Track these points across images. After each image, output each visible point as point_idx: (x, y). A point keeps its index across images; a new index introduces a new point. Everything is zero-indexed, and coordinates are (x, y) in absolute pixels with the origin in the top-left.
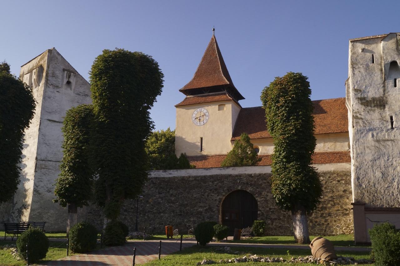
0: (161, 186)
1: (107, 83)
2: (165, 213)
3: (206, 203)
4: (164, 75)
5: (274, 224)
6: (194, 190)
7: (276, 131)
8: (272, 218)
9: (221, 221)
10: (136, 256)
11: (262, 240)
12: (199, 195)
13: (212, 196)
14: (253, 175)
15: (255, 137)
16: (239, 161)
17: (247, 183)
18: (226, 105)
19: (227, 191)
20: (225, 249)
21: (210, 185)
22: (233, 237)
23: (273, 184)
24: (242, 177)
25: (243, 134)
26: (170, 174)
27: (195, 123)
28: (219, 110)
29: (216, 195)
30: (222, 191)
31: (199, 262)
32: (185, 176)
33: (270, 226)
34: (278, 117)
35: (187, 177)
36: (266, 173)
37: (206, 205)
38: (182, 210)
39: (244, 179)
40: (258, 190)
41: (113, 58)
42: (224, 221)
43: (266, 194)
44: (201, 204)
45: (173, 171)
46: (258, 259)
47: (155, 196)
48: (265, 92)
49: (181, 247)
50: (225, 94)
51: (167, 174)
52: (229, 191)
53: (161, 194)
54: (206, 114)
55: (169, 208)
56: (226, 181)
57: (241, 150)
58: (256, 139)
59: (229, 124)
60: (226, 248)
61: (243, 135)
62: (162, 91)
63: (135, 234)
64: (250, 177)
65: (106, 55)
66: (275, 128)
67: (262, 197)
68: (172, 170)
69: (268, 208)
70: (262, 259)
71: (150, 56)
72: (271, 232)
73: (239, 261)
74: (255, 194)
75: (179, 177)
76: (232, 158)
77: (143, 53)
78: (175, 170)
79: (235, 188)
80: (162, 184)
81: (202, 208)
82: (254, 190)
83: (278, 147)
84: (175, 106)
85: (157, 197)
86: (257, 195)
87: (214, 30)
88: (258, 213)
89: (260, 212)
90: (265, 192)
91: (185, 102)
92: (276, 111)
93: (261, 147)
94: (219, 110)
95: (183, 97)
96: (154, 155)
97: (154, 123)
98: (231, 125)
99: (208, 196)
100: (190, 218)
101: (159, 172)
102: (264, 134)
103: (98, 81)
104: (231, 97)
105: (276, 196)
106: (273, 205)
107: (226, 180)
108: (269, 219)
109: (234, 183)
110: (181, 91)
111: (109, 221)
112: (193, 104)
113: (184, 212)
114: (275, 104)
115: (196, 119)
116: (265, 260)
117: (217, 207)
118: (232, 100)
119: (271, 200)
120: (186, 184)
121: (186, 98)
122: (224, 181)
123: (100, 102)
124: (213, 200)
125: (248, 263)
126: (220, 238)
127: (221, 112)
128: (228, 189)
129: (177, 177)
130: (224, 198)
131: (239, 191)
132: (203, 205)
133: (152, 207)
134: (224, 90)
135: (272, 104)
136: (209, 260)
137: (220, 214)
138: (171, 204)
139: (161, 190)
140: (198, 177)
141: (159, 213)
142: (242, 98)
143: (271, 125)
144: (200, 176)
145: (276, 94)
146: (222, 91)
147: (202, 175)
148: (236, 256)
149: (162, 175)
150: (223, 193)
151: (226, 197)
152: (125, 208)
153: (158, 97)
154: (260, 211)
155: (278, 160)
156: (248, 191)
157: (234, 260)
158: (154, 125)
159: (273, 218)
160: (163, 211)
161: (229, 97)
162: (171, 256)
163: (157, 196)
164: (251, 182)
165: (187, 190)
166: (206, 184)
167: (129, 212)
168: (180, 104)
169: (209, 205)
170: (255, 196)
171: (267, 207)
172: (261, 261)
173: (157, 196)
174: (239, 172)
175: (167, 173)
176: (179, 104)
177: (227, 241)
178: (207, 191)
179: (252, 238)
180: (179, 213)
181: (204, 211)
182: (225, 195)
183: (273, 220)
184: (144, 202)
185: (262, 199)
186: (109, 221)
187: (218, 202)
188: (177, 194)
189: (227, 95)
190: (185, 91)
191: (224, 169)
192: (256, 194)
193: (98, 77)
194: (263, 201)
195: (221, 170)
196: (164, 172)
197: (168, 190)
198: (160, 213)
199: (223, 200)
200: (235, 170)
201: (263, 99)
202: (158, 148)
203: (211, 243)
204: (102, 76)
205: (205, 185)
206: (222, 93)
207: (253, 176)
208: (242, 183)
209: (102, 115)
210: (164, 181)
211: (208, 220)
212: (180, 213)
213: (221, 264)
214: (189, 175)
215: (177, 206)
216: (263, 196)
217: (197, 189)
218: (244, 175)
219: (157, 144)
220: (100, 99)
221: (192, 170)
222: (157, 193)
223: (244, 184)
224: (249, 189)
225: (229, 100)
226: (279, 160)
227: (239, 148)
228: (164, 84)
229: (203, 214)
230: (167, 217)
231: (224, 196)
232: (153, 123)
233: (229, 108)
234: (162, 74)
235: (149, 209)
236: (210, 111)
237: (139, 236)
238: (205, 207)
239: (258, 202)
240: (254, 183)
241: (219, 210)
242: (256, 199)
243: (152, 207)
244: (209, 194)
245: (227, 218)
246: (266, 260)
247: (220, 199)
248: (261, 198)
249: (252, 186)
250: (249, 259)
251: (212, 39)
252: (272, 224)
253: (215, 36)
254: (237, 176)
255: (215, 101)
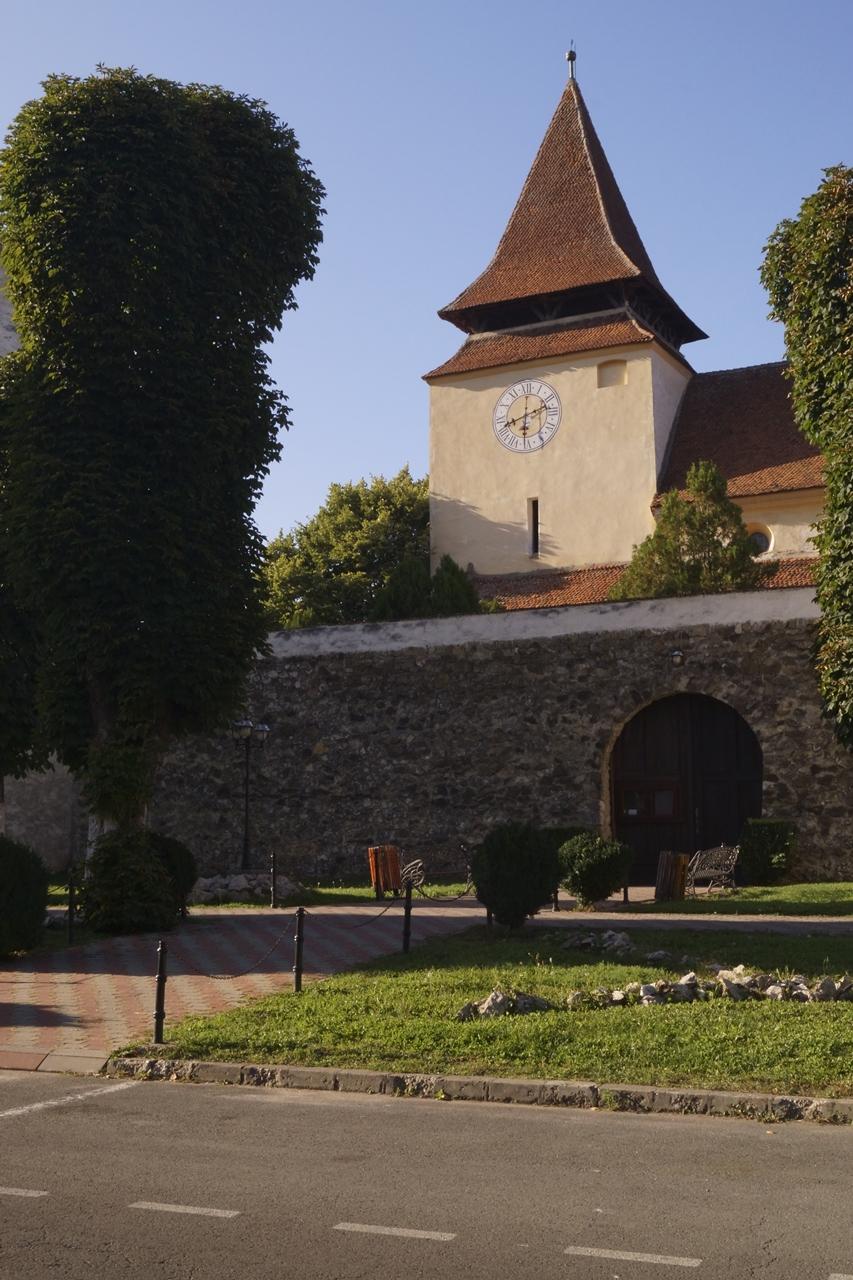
0: (360, 688)
1: (63, 221)
2: (376, 798)
3: (547, 754)
4: (324, 189)
5: (833, 831)
6: (494, 702)
7: (832, 417)
8: (822, 807)
9: (611, 825)
10: (169, 978)
11: (780, 898)
12: (515, 718)
13: (570, 723)
14: (738, 630)
15: (753, 489)
16: (681, 578)
17: (716, 666)
18: (629, 364)
19: (631, 700)
20: (605, 941)
21: (561, 679)
22: (654, 888)
23: (825, 650)
24: (692, 641)
25: (697, 466)
26: (394, 638)
27: (507, 442)
28: (599, 387)
29: (586, 719)
30: (610, 703)
31: (470, 1005)
32: (456, 643)
33: (816, 840)
34: (842, 351)
35: (462, 647)
36: (795, 620)
37: (543, 760)
38: (448, 782)
39: (701, 647)
40: (761, 690)
41: (85, 109)
42: (619, 821)
43: (796, 705)
44: (524, 759)
45: (405, 626)
46: (753, 984)
47: (336, 730)
48: (781, 245)
49: (407, 934)
50: (624, 318)
51: (381, 639)
52: (638, 701)
53: (362, 719)
54: (551, 403)
55: (395, 776)
56: (625, 661)
57: (688, 533)
58: (754, 495)
59: (643, 438)
60: (610, 937)
61: (697, 470)
62: (316, 260)
63: (240, 881)
64: (726, 639)
65: (56, 100)
66: (829, 402)
67: (778, 719)
68: (401, 623)
69: (804, 764)
70: (771, 987)
71: (256, 102)
72: (818, 868)
73: (660, 996)
74: (748, 707)
75: (431, 650)
76: (650, 567)
77: (226, 87)
78: (414, 622)
79: (666, 685)
80: (363, 679)
81: (526, 775)
82: (744, 694)
83: (845, 486)
84: (424, 378)
85: (345, 733)
86: (756, 713)
87: (572, 57)
88: (764, 788)
89: (772, 784)
90: (793, 700)
91: (463, 360)
92: (830, 324)
93: (777, 527)
94: (601, 384)
95: (453, 340)
96: (349, 577)
97: (286, 397)
98: (653, 443)
99: (551, 723)
100: (481, 813)
101: (348, 630)
102: (788, 474)
103: (26, 215)
104: (648, 330)
105: (837, 703)
106: (827, 753)
107: (627, 653)
108: (810, 810)
109: (658, 667)
110: (445, 315)
111: (109, 826)
112: (490, 367)
113: (454, 791)
114: (827, 294)
115: (508, 425)
116: (784, 993)
117: (590, 769)
118: (654, 342)
119: (818, 732)
120: (461, 676)
121: (468, 345)
122: (616, 659)
123: (43, 311)
124: (571, 738)
125: (705, 1004)
126: (594, 889)
127: (609, 391)
128: (634, 693)
129: (421, 649)
130: (618, 729)
131: (679, 697)
132: (531, 761)
133: (327, 774)
134: (621, 304)
135: (814, 293)
136: (518, 994)
137: (604, 798)
138: (403, 762)
139: (361, 704)
140: (510, 645)
141: (352, 799)
142: (696, 334)
143: (809, 391)
144: (516, 643)
145: (832, 244)
146: (612, 307)
147: (525, 636)
148: (649, 971)
149: (363, 642)
150: (613, 707)
151: (626, 725)
152: (219, 781)
153: (301, 290)
154: (773, 778)
155: (844, 543)
156: (719, 697)
157: (637, 990)
158: (285, 410)
159: (829, 806)
160: (372, 790)
161: (640, 330)
162: (354, 980)
163: (346, 729)
164: (731, 661)
165: (465, 702)
166: (542, 674)
167: (237, 795)
168: (443, 367)
169: (556, 760)
170: (748, 719)
171: (803, 761)
172: (764, 997)
173: (346, 729)
174: (682, 617)
175: (384, 636)
176: (440, 368)
177: (627, 906)
178: (548, 701)
179: (736, 893)
180: (434, 794)
181: (537, 785)
182: (623, 717)
183: (827, 818)
184: (293, 754)
185: (780, 729)
186: (109, 826)
187: (592, 749)
188: (423, 720)
189: (634, 322)
190: (461, 316)
191: (617, 609)
192: (754, 708)
193: (24, 199)
194: (784, 739)
195: (602, 613)
196: (369, 632)
197: (388, 704)
198: (359, 797)
199: (613, 739)
200: (662, 610)
201: (772, 278)
202: (362, 548)
203: (546, 914)
204: (40, 192)
205: (540, 677)
206: (612, 316)
207: (738, 636)
208: (692, 663)
209: (52, 370)
210: (370, 667)
211: (556, 821)
212: (440, 797)
213: (574, 1009)
214: (470, 639)
215: (426, 768)
216: (783, 719)
217: (506, 698)
218: (700, 630)
219: (358, 534)
220: (43, 297)
221: (484, 618)
222: (344, 719)
223: (702, 667)
224: (725, 691)
225: (642, 342)
226: (847, 545)
227: (679, 524)
228: (327, 224)
229: (534, 796)
230: (387, 811)
231: (617, 720)
232: (283, 402)
233: (640, 373)
234: (317, 183)
235: (315, 782)
236: (565, 392)
237: (258, 891)
238: (541, 767)
239: (762, 741)
240: (741, 663)
241: (600, 782)
242: (755, 729)
243: (327, 774)
244: (555, 714)
245: (633, 812)
246: (791, 988)
247: (601, 732)
248: (775, 727)
249: (735, 678)
250: (709, 988)
251: (567, 96)
252: (825, 833)
253: (577, 81)
254: (670, 635)
255: (586, 350)
